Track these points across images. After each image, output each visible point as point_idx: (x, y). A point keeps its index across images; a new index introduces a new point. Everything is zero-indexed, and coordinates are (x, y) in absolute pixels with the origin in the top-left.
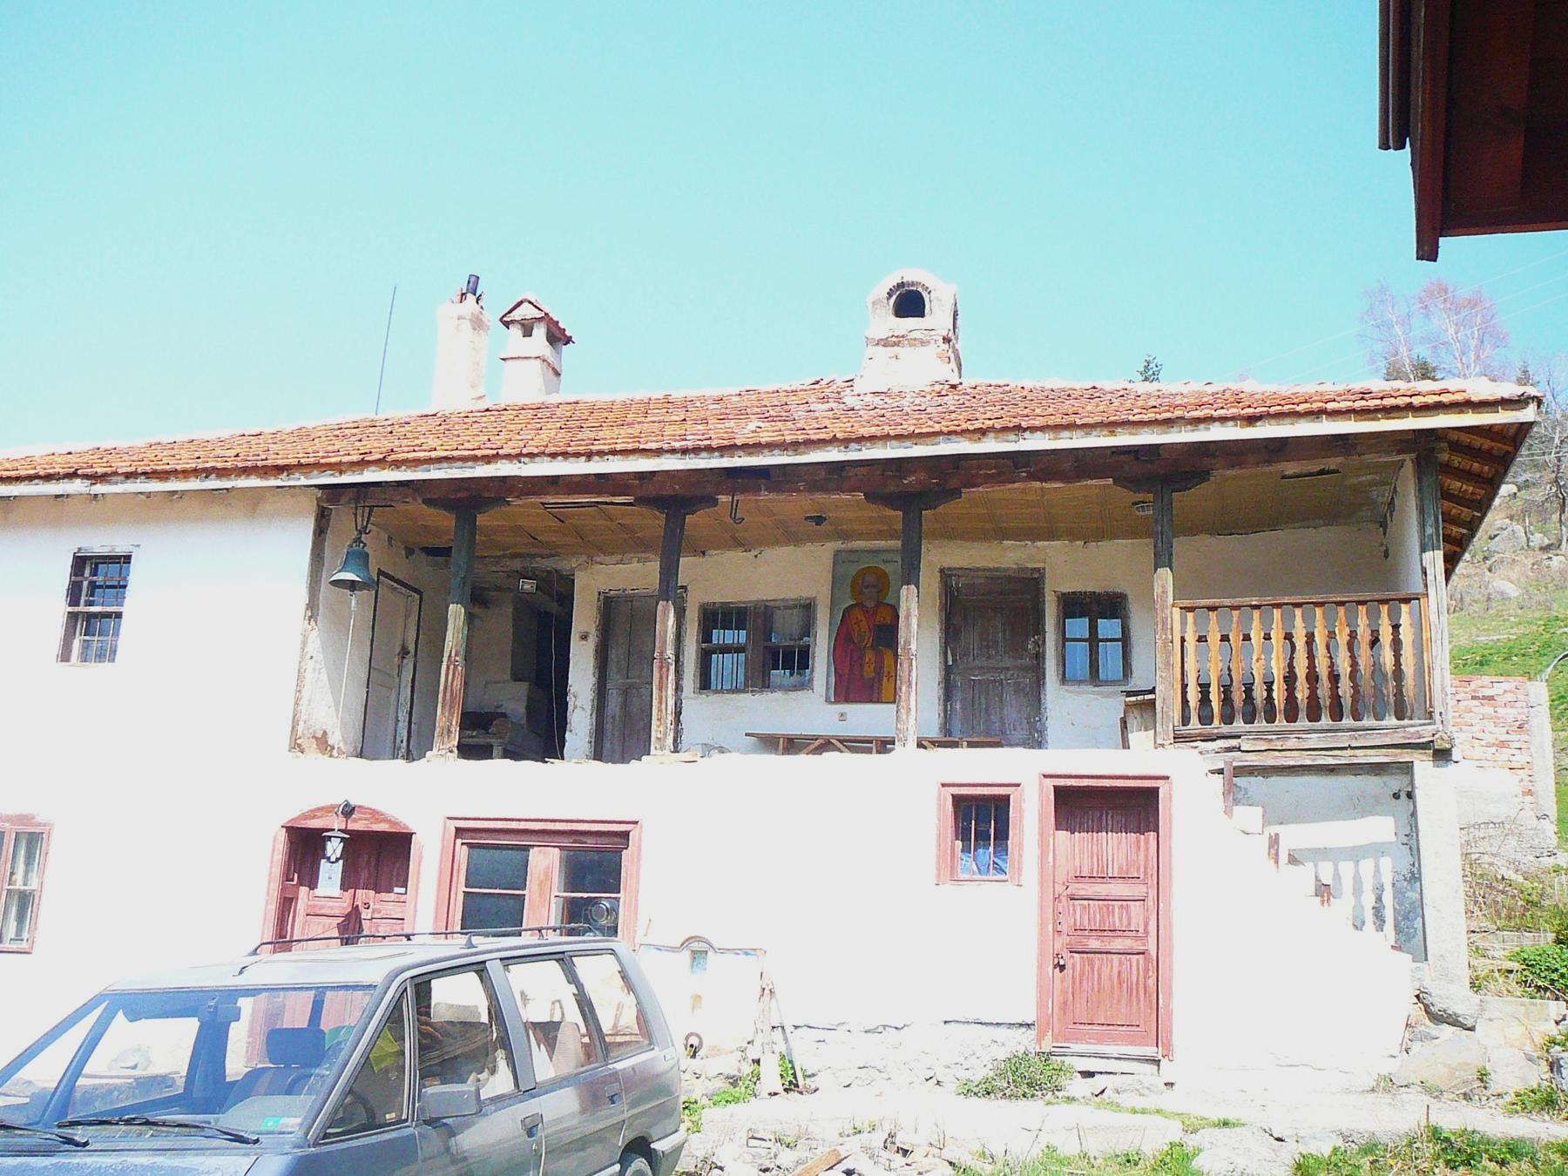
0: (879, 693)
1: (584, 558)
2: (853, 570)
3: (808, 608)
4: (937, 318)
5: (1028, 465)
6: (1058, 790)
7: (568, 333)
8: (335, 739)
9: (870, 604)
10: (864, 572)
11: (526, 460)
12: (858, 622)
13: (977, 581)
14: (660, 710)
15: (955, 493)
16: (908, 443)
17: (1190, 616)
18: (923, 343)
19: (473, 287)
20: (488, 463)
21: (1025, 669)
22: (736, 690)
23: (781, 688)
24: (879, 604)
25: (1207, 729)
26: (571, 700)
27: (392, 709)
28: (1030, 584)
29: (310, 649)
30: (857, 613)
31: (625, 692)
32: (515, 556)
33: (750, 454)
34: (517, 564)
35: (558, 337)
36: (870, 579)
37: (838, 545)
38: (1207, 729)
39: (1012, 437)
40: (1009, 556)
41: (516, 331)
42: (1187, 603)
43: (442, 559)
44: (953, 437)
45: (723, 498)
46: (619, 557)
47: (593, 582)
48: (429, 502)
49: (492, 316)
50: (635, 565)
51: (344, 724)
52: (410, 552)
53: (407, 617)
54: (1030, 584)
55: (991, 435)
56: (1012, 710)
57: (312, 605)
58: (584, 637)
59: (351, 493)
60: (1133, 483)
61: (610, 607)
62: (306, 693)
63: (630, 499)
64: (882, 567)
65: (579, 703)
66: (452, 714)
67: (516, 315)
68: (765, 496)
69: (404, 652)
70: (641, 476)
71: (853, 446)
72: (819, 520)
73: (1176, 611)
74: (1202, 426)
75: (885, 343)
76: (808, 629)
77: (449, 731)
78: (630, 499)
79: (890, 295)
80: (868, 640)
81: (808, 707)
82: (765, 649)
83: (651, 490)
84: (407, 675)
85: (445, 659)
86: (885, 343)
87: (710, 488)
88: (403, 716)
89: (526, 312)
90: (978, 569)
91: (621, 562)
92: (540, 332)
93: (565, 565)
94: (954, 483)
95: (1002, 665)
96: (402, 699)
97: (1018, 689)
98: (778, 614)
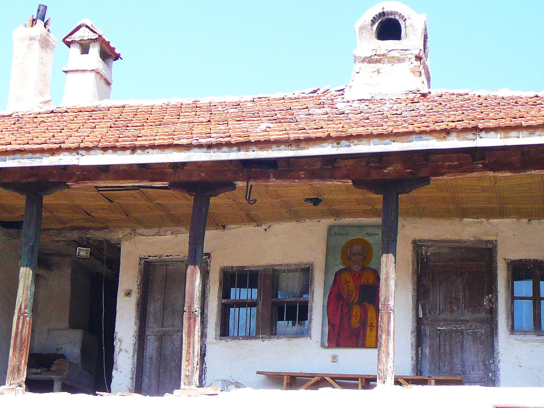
0: (364, 340)
2: (343, 241)
3: (307, 271)
4: (411, 40)
5: (483, 159)
7: (117, 51)
9: (356, 268)
10: (351, 243)
11: (83, 152)
12: (347, 282)
13: (443, 251)
19: (42, 14)
21: (482, 321)
28: (485, 253)
30: (347, 277)
31: (161, 338)
32: (73, 228)
33: (261, 149)
34: (75, 235)
35: (109, 54)
36: (357, 248)
37: (331, 221)
39: (471, 136)
41: (75, 50)
43: (13, 231)
45: (240, 184)
46: (157, 230)
47: (136, 249)
50: (169, 237)
54: (485, 253)
56: (471, 354)
58: (128, 294)
61: (148, 269)
63: (165, 184)
64: (367, 238)
65: (123, 347)
66: (21, 356)
67: (76, 36)
71: (344, 142)
75: (369, 60)
76: (307, 288)
77: (19, 370)
79: (373, 22)
80: (355, 297)
82: (269, 302)
83: (182, 177)
85: (16, 311)
86: (369, 60)
89: (84, 34)
90: (443, 241)
91: (158, 234)
92: (95, 50)
93: (114, 236)
94: (424, 172)
95: (462, 318)
98: (283, 276)
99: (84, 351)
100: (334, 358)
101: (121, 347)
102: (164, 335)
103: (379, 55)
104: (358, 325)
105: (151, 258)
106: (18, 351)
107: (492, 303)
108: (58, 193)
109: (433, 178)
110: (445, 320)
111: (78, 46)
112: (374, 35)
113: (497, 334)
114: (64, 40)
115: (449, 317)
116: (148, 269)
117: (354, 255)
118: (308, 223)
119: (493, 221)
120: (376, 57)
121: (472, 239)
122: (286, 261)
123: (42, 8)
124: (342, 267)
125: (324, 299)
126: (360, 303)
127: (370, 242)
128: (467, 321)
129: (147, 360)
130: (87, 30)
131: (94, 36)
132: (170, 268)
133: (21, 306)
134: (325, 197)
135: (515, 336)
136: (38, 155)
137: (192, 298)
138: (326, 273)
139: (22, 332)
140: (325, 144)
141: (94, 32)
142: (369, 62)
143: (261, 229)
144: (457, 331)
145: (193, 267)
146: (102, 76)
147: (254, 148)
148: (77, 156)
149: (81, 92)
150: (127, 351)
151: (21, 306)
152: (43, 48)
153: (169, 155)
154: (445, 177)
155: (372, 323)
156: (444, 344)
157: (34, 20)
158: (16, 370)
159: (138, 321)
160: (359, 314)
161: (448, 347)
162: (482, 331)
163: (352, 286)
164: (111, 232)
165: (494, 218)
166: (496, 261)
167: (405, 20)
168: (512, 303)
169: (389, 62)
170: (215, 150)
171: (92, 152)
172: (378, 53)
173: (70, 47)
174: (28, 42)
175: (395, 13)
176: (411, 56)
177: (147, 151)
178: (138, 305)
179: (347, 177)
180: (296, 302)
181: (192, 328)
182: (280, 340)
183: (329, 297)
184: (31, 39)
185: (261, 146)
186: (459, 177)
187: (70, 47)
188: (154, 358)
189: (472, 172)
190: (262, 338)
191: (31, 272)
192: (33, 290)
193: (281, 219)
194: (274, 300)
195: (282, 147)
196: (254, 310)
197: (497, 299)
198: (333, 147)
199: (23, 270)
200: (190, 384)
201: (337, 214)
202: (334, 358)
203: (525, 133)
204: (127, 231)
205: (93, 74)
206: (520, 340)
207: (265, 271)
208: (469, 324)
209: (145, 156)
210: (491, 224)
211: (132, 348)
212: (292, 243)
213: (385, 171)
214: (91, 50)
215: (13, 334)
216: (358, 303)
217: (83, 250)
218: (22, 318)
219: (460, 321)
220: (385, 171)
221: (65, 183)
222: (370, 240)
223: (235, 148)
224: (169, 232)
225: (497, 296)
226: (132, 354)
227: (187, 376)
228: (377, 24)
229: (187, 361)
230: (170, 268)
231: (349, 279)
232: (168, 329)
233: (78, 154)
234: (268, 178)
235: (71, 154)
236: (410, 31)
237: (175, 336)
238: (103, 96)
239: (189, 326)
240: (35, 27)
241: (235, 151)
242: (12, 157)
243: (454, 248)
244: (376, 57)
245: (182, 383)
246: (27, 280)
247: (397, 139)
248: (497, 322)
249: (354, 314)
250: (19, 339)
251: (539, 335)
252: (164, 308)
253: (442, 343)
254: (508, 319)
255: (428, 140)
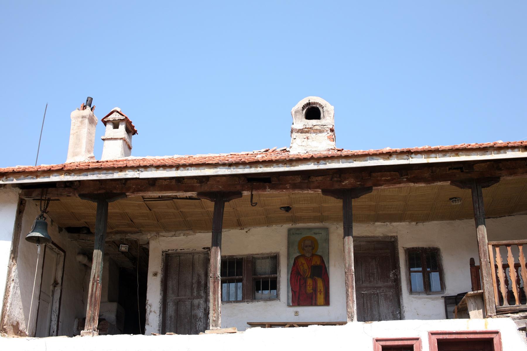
0: (316, 300)
1: (156, 234)
2: (298, 238)
3: (275, 258)
4: (328, 119)
5: (407, 175)
6: (439, 342)
7: (135, 129)
8: (22, 327)
9: (308, 255)
10: (304, 239)
11: (142, 169)
12: (302, 264)
13: (362, 243)
14: (214, 305)
15: (369, 189)
16: (351, 160)
17: (497, 249)
18: (321, 132)
19: (89, 103)
20: (121, 171)
21: (390, 287)
22: (237, 301)
23: (261, 299)
24: (313, 255)
25: (513, 307)
26: (148, 308)
27: (49, 314)
28: (390, 244)
29: (13, 274)
30: (302, 260)
31: (177, 304)
32: (117, 232)
33: (266, 166)
34: (118, 237)
35: (131, 130)
36: (308, 243)
37: (289, 226)
38: (513, 307)
39: (405, 157)
40: (379, 230)
41: (110, 126)
42: (495, 243)
43: (76, 235)
44: (374, 157)
45: (246, 193)
46: (173, 233)
47: (159, 246)
48: (82, 196)
49: (98, 119)
50: (182, 237)
51: (26, 319)
52: (60, 230)
53: (57, 264)
54: (390, 244)
55: (394, 156)
56: (384, 307)
57: (14, 253)
58: (155, 274)
59: (36, 193)
60: (462, 184)
61: (168, 258)
62: (9, 300)
63: (193, 194)
64: (314, 236)
65: (153, 309)
66: (95, 309)
67: (111, 118)
68: (268, 192)
69: (56, 284)
70: (207, 178)
71: (322, 162)
72: (288, 209)
73: (491, 247)
74: (502, 151)
75: (301, 131)
76: (275, 269)
77: (94, 319)
78: (193, 194)
79: (303, 108)
80: (308, 274)
81: (280, 307)
82: (251, 279)
83: (206, 188)
84: (57, 296)
85: (91, 279)
86: (301, 131)
87: (238, 188)
88: (54, 318)
89: (115, 116)
90: (363, 237)
91: (174, 235)
92: (122, 127)
93: (143, 238)
94: (369, 184)
95: (377, 285)
96: (54, 308)
97: (386, 298)
98: (258, 262)
99: (118, 316)
100: (296, 313)
101: (151, 309)
102: (179, 301)
103: (308, 128)
104: (311, 291)
105: (170, 251)
106: (93, 306)
107: (397, 275)
108: (121, 201)
109: (374, 188)
110: (366, 287)
111: (112, 124)
112: (304, 117)
113: (401, 294)
114: (103, 120)
115: (368, 285)
116: (168, 258)
117: (306, 246)
118: (274, 227)
119: (395, 224)
120: (306, 129)
121: (382, 235)
122: (261, 252)
123: (89, 99)
124: (298, 254)
125: (288, 275)
126: (312, 277)
127: (316, 238)
128: (380, 287)
129: (168, 318)
130: (118, 114)
131: (122, 118)
132: (182, 258)
133: (95, 276)
134: (294, 206)
135: (413, 296)
136: (110, 172)
137: (216, 268)
138: (288, 259)
139: (95, 293)
140: (309, 163)
141: (122, 115)
142: (301, 133)
143: (244, 231)
144: (374, 294)
145: (215, 248)
146: (127, 142)
147: (261, 166)
148: (138, 172)
149: (113, 152)
150: (155, 312)
151: (95, 276)
152: (90, 123)
153: (202, 171)
154: (383, 187)
155: (320, 290)
156: (367, 303)
157: (84, 106)
158: (91, 320)
159: (162, 292)
160: (311, 284)
161: (369, 305)
162: (390, 293)
163: (306, 266)
164: (143, 234)
165: (394, 222)
166: (398, 249)
167: (323, 108)
168: (410, 275)
169: (314, 133)
170: (234, 167)
171: (148, 169)
172: (307, 127)
173: (105, 125)
174: (80, 119)
175: (317, 103)
176: (327, 129)
177: (187, 168)
178: (162, 282)
179: (318, 187)
180: (268, 278)
181: (216, 288)
182: (259, 303)
183: (291, 274)
184: (83, 117)
185: (266, 164)
186: (391, 187)
187: (105, 125)
188: (173, 317)
189: (400, 183)
190: (247, 302)
191: (101, 253)
192: (102, 265)
193: (258, 223)
194: (254, 276)
195: (280, 165)
196: (240, 284)
197: (400, 272)
198: (315, 165)
199: (95, 252)
200: (216, 326)
201: (294, 220)
202: (296, 313)
203: (441, 155)
204: (153, 234)
205: (122, 141)
206: (416, 298)
207: (247, 258)
208: (382, 289)
209: (186, 171)
210: (393, 226)
211: (159, 310)
212: (262, 240)
213: (343, 184)
214: (120, 126)
215: (89, 295)
216: (310, 277)
217: (124, 247)
218: (95, 284)
219: (376, 287)
220: (343, 184)
221: (124, 194)
222: (317, 237)
223: (248, 166)
224: (182, 234)
225: (400, 271)
226: (158, 314)
227: (214, 321)
228: (305, 110)
229: (214, 310)
230: (182, 258)
231: (304, 262)
232: (182, 297)
233: (139, 171)
234: (265, 188)
235: (134, 171)
236: (326, 114)
237: (187, 302)
238: (127, 155)
239: (214, 287)
240: (85, 111)
241: (248, 168)
242: (92, 173)
243: (369, 242)
244: (306, 129)
245: (211, 325)
246: (98, 258)
247: (357, 159)
248: (401, 287)
249: (308, 284)
250: (93, 299)
251: (428, 294)
252: (179, 284)
253: (365, 302)
254: (407, 284)
255: (378, 160)
